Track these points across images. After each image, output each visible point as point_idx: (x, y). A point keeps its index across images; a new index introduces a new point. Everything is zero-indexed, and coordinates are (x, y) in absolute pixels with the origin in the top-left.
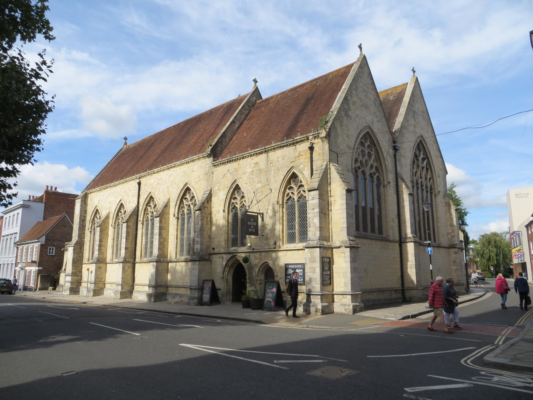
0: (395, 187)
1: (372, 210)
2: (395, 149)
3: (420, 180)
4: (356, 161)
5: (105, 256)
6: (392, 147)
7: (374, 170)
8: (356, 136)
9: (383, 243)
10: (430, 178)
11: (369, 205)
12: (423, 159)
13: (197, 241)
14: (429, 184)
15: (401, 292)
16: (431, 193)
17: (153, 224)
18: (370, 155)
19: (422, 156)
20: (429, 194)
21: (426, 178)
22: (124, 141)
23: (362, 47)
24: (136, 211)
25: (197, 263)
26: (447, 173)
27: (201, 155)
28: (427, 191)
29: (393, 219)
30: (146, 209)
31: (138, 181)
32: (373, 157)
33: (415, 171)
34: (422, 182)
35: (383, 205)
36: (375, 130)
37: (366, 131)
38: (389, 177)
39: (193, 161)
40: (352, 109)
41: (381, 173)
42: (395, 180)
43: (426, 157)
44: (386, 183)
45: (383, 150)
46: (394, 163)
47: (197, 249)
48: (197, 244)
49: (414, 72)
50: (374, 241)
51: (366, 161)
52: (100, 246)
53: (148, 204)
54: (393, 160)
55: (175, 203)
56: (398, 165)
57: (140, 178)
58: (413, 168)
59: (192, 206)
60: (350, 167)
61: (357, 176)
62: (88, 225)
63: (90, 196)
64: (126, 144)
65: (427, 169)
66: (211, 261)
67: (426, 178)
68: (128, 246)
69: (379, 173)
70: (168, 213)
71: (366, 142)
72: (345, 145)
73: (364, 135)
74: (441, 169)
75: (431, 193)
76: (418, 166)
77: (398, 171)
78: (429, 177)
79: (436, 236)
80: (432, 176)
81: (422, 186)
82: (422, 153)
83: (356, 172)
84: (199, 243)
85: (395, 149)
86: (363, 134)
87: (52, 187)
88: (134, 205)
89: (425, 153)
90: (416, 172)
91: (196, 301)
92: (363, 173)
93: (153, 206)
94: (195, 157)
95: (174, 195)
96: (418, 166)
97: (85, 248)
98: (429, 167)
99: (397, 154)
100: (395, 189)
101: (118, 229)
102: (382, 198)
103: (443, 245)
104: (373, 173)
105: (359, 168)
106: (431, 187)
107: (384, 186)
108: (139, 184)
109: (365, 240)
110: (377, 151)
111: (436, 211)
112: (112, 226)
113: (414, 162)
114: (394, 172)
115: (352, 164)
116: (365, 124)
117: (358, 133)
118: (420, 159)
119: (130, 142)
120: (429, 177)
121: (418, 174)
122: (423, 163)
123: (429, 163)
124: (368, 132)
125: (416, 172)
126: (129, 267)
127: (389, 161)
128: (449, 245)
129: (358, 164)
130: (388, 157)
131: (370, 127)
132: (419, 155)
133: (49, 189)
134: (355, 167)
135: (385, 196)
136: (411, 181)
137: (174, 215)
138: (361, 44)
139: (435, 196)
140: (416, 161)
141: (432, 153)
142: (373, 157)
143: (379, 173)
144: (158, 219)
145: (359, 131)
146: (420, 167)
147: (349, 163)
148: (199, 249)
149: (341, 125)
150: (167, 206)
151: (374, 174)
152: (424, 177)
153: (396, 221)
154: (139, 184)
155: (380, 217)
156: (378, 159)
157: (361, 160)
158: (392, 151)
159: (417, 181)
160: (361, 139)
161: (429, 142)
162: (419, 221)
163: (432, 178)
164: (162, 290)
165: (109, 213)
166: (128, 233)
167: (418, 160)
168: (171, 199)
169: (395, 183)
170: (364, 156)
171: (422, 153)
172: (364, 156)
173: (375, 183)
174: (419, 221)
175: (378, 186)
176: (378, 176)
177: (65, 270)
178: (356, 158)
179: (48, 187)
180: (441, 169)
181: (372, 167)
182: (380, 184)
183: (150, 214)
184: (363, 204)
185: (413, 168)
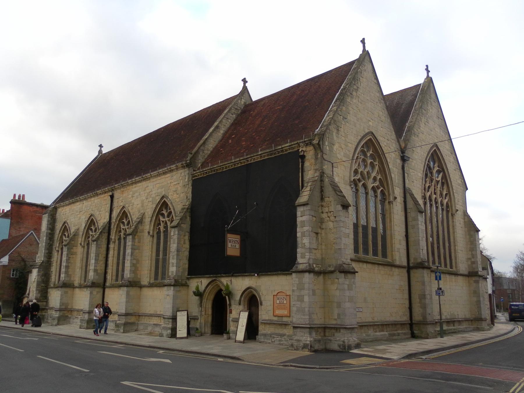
0: (403, 203)
1: (375, 230)
2: (404, 159)
3: (434, 196)
4: (356, 172)
5: (72, 279)
6: (399, 157)
7: (377, 184)
8: (356, 144)
9: (387, 269)
10: (446, 195)
11: (372, 224)
12: (438, 172)
13: (173, 263)
14: (445, 202)
15: (408, 326)
16: (448, 212)
17: (125, 243)
18: (372, 165)
19: (436, 169)
20: (445, 212)
21: (441, 194)
22: (99, 148)
23: (366, 42)
24: (107, 228)
25: (172, 288)
26: (478, 231)
27: (179, 165)
28: (443, 209)
29: (400, 240)
30: (118, 226)
31: (110, 194)
32: (377, 168)
33: (427, 185)
34: (436, 198)
35: (388, 225)
36: (380, 139)
37: (369, 138)
38: (396, 192)
39: (171, 171)
40: (351, 112)
41: (386, 187)
42: (402, 195)
43: (442, 170)
44: (392, 199)
45: (388, 160)
46: (401, 176)
47: (173, 272)
48: (173, 266)
49: (428, 71)
50: (376, 266)
51: (368, 173)
52: (67, 267)
53: (121, 221)
54: (401, 171)
55: (150, 219)
56: (406, 178)
57: (113, 190)
58: (426, 182)
59: (169, 223)
60: (347, 179)
61: (357, 190)
62: (56, 244)
63: (59, 210)
64: (100, 152)
65: (443, 184)
66: (188, 286)
67: (441, 194)
68: (98, 268)
69: (384, 187)
70: (142, 231)
71: (368, 151)
72: (342, 154)
73: (366, 143)
74: (459, 185)
75: (448, 212)
76: (432, 180)
77: (407, 185)
78: (444, 193)
79: (454, 261)
80: (449, 191)
81: (436, 203)
82: (436, 165)
83: (356, 185)
84: (175, 265)
85: (404, 159)
86: (365, 141)
87: (19, 196)
88: (107, 219)
89: (440, 166)
90: (429, 187)
91: (169, 331)
92: (364, 186)
93: (126, 223)
94: (173, 167)
95: (150, 210)
96: (432, 180)
97: (52, 270)
98: (446, 181)
99: (406, 165)
100: (403, 205)
101: (88, 248)
102: (387, 216)
103: (461, 272)
104: (377, 186)
105: (359, 180)
106: (447, 206)
107: (389, 202)
108: (112, 197)
109: (365, 264)
110: (381, 163)
111: (454, 232)
112: (81, 244)
113: (426, 175)
114: (401, 186)
115: (350, 176)
116: (367, 131)
117: (358, 141)
118: (434, 171)
119: (105, 151)
120: (444, 193)
121: (432, 189)
122: (438, 177)
123: (445, 177)
124: (370, 139)
125: (429, 187)
126: (98, 292)
127: (396, 173)
128: (469, 272)
129: (359, 176)
130: (395, 169)
131: (372, 133)
132: (434, 167)
133: (17, 198)
134: (354, 180)
135: (390, 213)
136: (423, 196)
137: (149, 233)
138: (364, 39)
139: (452, 215)
140: (429, 175)
141: (449, 166)
142: (377, 168)
143: (384, 187)
144: (131, 237)
145: (359, 138)
146: (434, 181)
147: (348, 174)
148: (175, 272)
149: (338, 130)
150: (141, 221)
151: (378, 187)
152: (438, 193)
153: (404, 243)
154: (112, 197)
155: (384, 237)
156: (384, 170)
157: (361, 172)
158: (399, 162)
159: (430, 197)
160: (363, 147)
161: (444, 149)
162: (432, 244)
163: (448, 194)
164: (132, 319)
165: (78, 229)
166: (97, 255)
167: (431, 173)
168: (146, 213)
169: (403, 199)
170: (366, 166)
171: (436, 165)
172: (366, 166)
173: (379, 197)
174: (432, 244)
175: (383, 201)
176: (382, 191)
177: (29, 294)
178: (356, 169)
179: (15, 195)
180: (459, 185)
181: (375, 179)
182: (385, 199)
183: (123, 232)
184: (363, 222)
185: (426, 182)
